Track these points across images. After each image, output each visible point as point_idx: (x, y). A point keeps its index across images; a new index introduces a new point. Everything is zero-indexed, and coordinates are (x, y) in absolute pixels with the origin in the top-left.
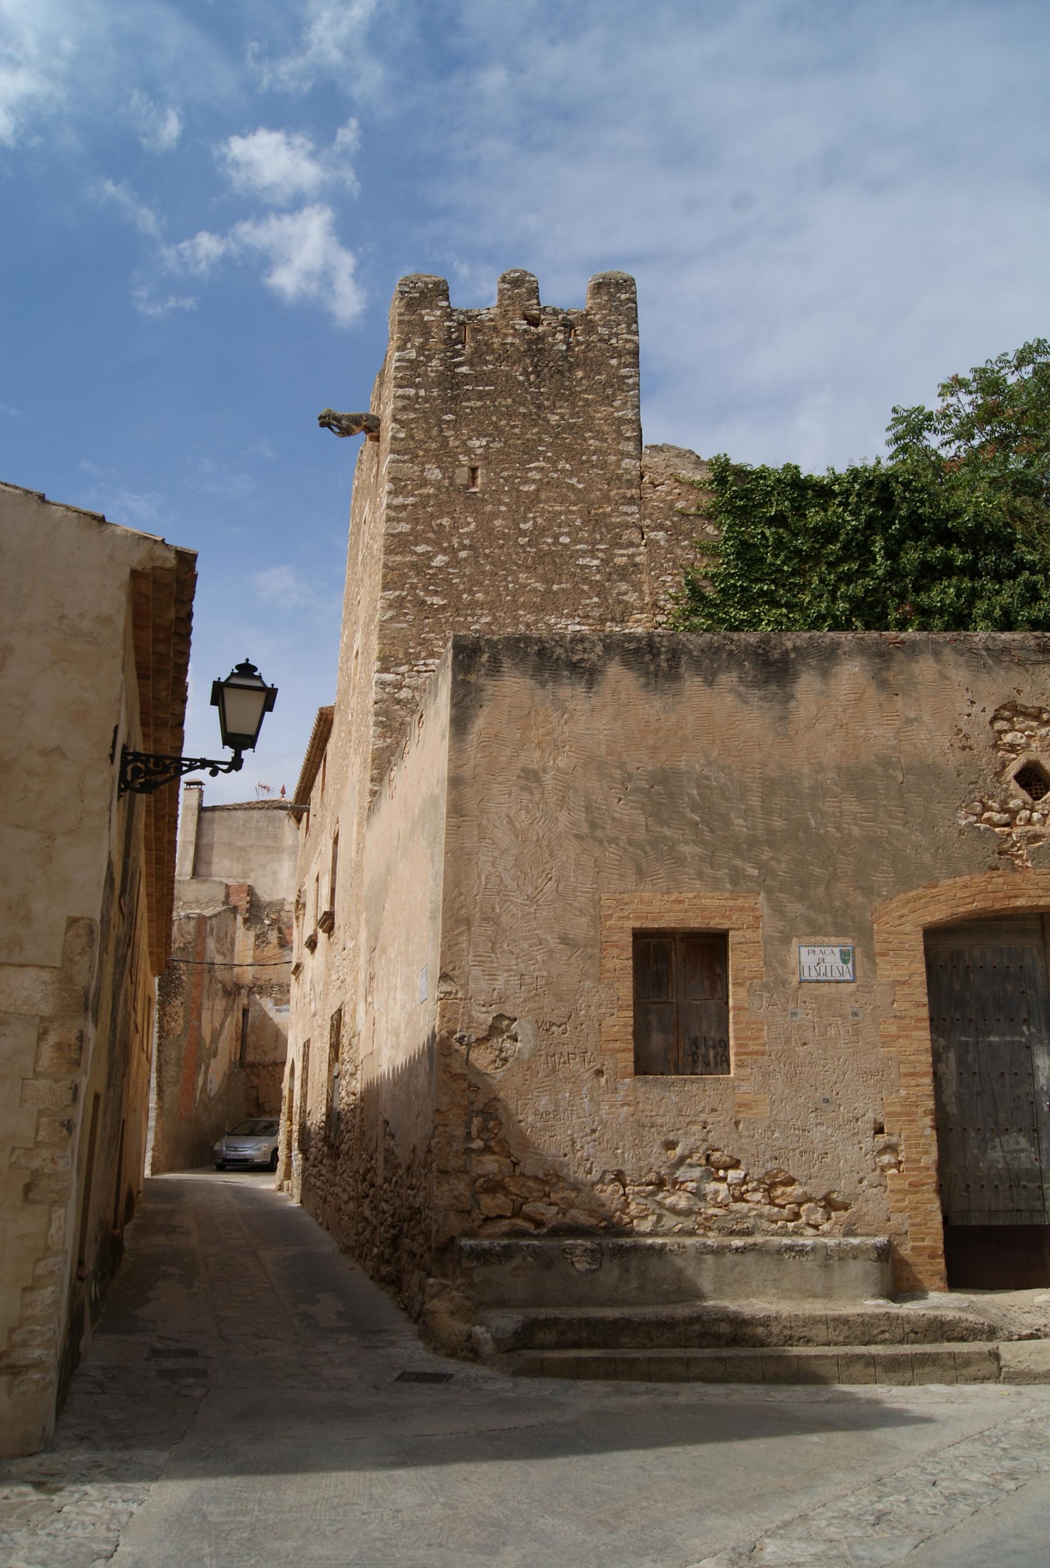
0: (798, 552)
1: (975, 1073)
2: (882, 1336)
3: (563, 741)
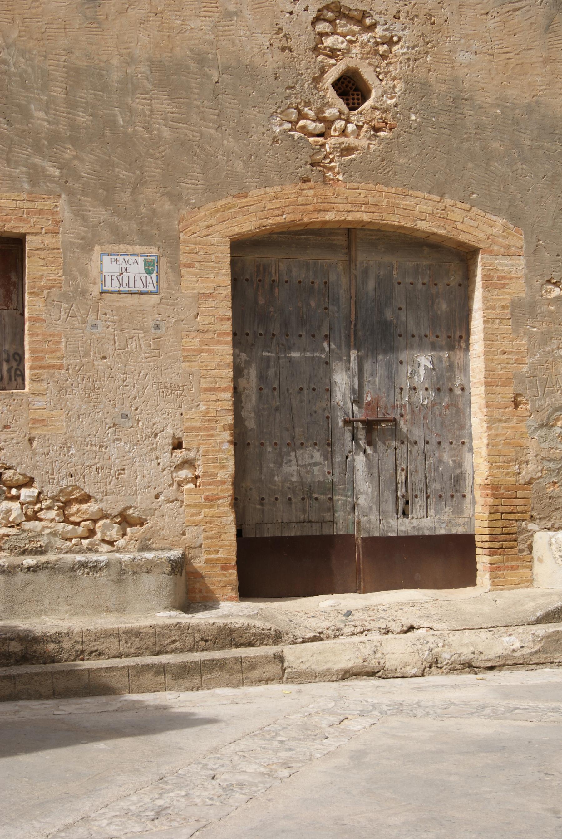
1: (274, 389)
2: (173, 646)
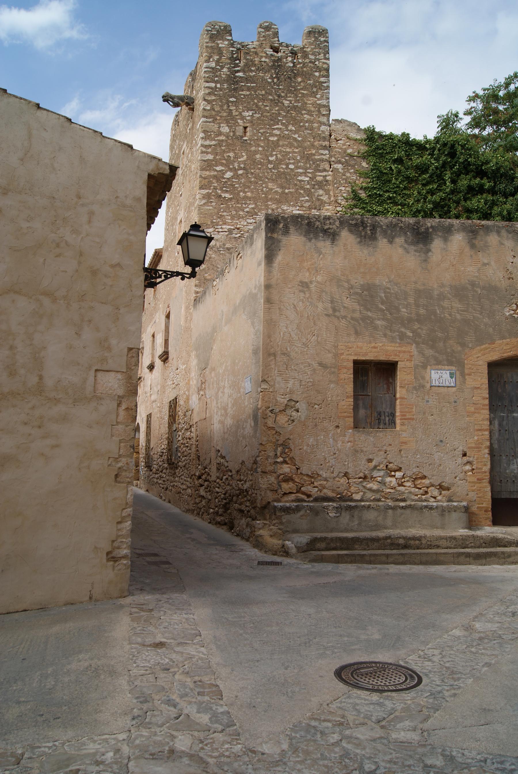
0: (408, 178)
1: (506, 430)
2: (470, 545)
3: (320, 268)
